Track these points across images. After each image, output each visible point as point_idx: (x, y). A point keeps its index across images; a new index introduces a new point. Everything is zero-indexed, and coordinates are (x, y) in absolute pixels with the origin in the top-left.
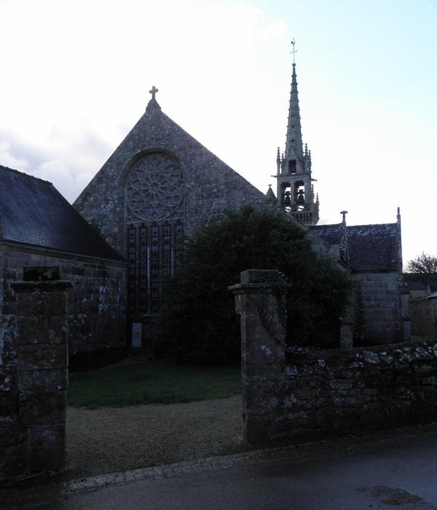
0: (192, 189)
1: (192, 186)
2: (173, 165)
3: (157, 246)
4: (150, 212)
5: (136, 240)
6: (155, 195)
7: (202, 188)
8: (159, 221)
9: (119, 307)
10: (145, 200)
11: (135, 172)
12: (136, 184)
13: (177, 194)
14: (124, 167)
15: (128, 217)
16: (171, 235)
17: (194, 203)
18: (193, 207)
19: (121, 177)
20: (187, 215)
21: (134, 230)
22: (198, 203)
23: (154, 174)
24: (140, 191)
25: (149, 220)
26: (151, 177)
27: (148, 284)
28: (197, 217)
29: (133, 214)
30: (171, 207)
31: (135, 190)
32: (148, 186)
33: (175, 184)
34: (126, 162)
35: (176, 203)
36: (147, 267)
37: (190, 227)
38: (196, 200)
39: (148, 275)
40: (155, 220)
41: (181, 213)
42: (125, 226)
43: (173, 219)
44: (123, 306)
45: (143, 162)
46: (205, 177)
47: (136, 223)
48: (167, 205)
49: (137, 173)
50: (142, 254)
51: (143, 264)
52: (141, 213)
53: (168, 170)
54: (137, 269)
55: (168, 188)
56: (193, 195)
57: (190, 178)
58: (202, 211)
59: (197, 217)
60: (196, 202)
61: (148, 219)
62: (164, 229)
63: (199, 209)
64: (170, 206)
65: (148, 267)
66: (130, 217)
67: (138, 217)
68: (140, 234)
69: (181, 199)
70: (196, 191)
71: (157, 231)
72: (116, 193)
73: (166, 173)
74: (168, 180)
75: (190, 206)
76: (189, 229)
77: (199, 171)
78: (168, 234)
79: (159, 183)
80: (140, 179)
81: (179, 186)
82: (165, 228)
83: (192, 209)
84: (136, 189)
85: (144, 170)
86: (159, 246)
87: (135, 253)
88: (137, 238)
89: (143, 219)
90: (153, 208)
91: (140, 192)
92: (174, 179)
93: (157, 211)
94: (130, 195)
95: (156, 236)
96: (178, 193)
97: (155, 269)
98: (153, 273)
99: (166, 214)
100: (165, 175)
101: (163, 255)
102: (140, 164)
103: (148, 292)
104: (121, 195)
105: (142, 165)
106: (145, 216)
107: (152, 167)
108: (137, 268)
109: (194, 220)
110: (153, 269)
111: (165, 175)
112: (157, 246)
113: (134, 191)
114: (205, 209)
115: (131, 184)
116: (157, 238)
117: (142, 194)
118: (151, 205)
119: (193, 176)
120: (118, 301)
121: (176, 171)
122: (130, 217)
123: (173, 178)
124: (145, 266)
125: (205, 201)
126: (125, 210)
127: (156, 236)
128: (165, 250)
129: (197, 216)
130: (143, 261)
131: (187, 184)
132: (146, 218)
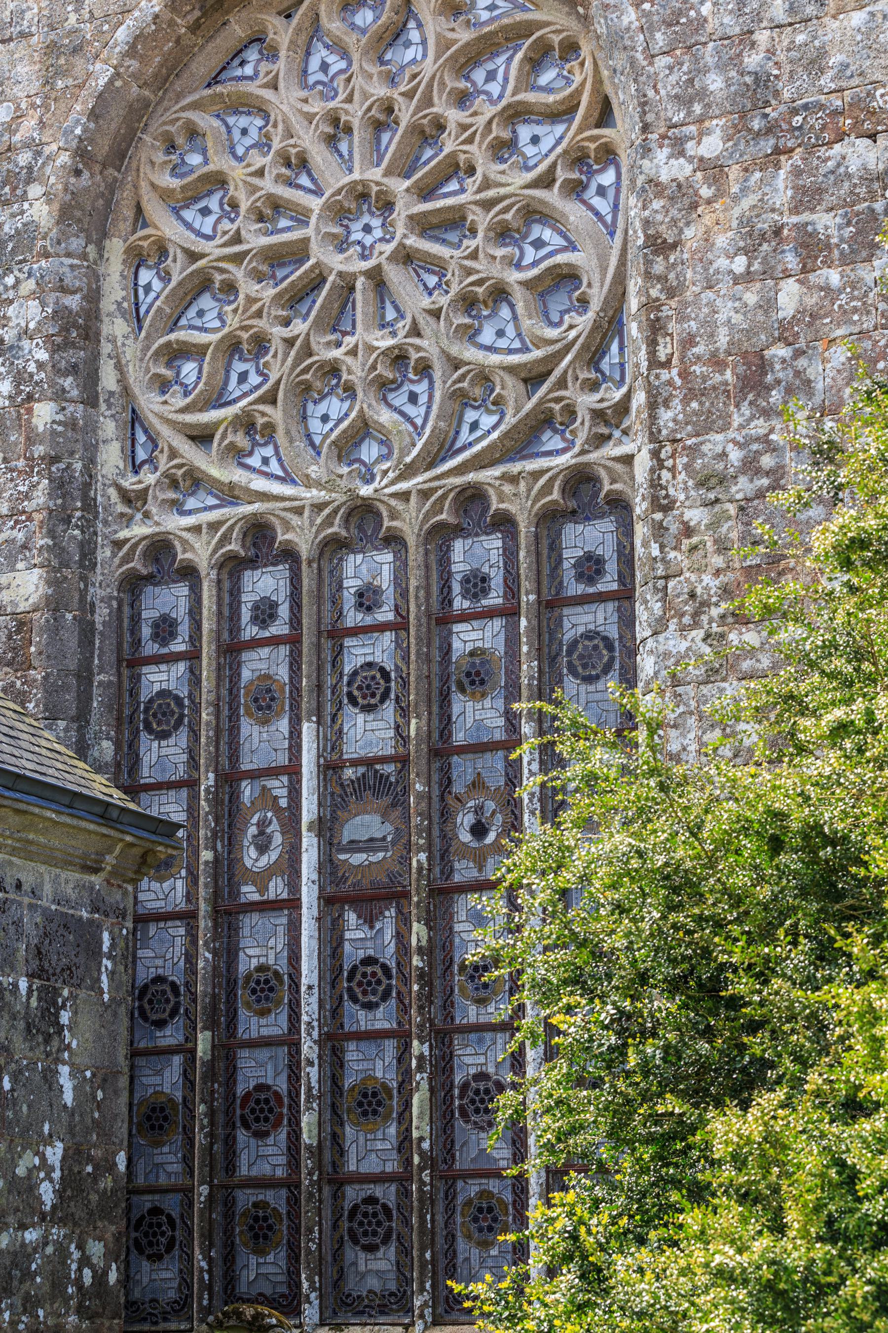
0: (706, 192)
1: (703, 164)
2: (524, 30)
3: (389, 710)
4: (316, 426)
5: (195, 679)
6: (360, 283)
7: (797, 172)
8: (404, 496)
9: (62, 1252)
10: (278, 332)
11: (193, 116)
12: (205, 212)
13: (560, 259)
14: (102, 74)
15: (129, 482)
16: (510, 612)
17: (726, 311)
18: (723, 339)
19: (81, 153)
20: (665, 416)
21: (182, 590)
22: (768, 304)
23: (355, 114)
24: (238, 258)
25: (315, 494)
26: (331, 141)
27: (308, 1048)
28: (759, 426)
29: (173, 454)
30: (511, 369)
31: (193, 256)
32: (301, 217)
33: (546, 181)
34: (122, 34)
35: (552, 333)
36: (293, 904)
37: (696, 515)
38: (748, 277)
39: (309, 972)
40: (366, 491)
41: (598, 415)
42: (104, 553)
43: (532, 465)
44: (96, 1249)
45: (258, 39)
46: (826, 81)
47: (196, 529)
48: (471, 354)
49: (205, 121)
50: (247, 791)
51: (261, 879)
52: (241, 440)
53: (479, 76)
54: (204, 923)
55: (482, 220)
56: (721, 241)
57: (683, 100)
58: (815, 370)
59: (759, 426)
60: (751, 298)
61: (309, 483)
62: (445, 562)
63: (781, 351)
64: (495, 359)
65: (309, 895)
66: (150, 478)
67: (215, 472)
68: (446, 587)
69: (597, 298)
70: (746, 203)
71: (385, 580)
72: (30, 285)
73: (462, 99)
74: (478, 153)
75: (689, 341)
76: (688, 531)
77: (762, 37)
78: (601, 587)
79: (400, 186)
80: (237, 172)
81: (576, 189)
82: (458, 546)
83: (717, 362)
84: (202, 246)
85: (268, 94)
86: (403, 711)
87: (191, 784)
88: (207, 650)
89: (260, 484)
90: (350, 390)
91: (238, 273)
92: (535, 140)
93: (385, 417)
94: (145, 301)
95: (381, 628)
96: (572, 247)
97: (370, 921)
98: (352, 954)
99: (465, 436)
100: (454, 116)
101: (447, 783)
102: (238, 55)
103: (308, 1121)
104: (73, 302)
105: (252, 55)
106: (274, 467)
107: (337, 64)
108: (203, 907)
109: (735, 456)
110: (351, 917)
111: (454, 116)
112: (389, 710)
113: (178, 270)
114: (839, 355)
115: (155, 210)
116: (388, 638)
117: (248, 287)
118: (333, 370)
119: (715, 83)
120: (47, 1193)
121: (547, 77)
122: (150, 478)
123: (525, 133)
124: (277, 889)
125: (834, 277)
126: (109, 428)
127: (381, 628)
128: (459, 737)
129: (767, 413)
130: (263, 849)
131: (662, 155)
132: (286, 479)
